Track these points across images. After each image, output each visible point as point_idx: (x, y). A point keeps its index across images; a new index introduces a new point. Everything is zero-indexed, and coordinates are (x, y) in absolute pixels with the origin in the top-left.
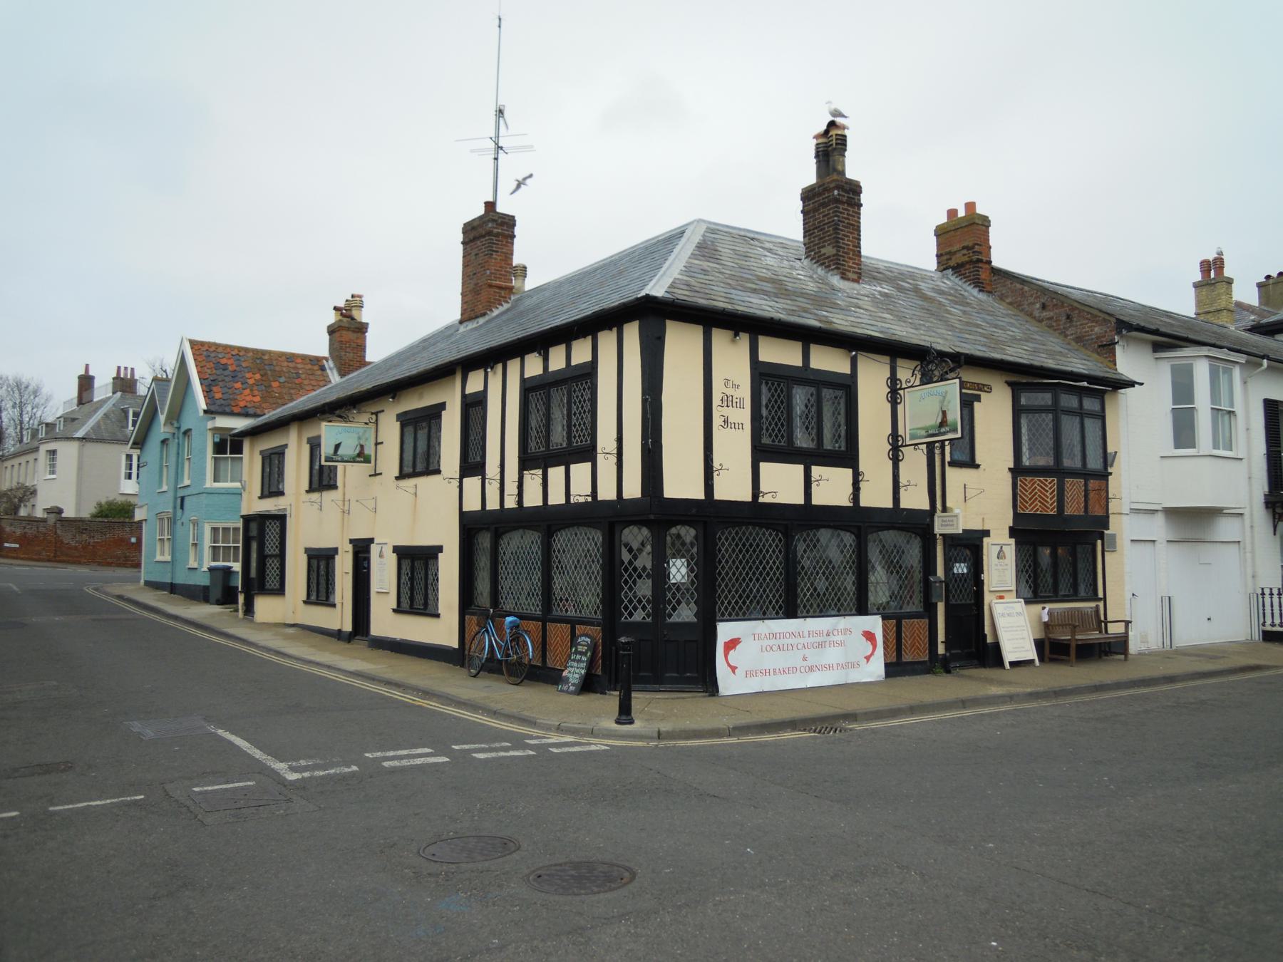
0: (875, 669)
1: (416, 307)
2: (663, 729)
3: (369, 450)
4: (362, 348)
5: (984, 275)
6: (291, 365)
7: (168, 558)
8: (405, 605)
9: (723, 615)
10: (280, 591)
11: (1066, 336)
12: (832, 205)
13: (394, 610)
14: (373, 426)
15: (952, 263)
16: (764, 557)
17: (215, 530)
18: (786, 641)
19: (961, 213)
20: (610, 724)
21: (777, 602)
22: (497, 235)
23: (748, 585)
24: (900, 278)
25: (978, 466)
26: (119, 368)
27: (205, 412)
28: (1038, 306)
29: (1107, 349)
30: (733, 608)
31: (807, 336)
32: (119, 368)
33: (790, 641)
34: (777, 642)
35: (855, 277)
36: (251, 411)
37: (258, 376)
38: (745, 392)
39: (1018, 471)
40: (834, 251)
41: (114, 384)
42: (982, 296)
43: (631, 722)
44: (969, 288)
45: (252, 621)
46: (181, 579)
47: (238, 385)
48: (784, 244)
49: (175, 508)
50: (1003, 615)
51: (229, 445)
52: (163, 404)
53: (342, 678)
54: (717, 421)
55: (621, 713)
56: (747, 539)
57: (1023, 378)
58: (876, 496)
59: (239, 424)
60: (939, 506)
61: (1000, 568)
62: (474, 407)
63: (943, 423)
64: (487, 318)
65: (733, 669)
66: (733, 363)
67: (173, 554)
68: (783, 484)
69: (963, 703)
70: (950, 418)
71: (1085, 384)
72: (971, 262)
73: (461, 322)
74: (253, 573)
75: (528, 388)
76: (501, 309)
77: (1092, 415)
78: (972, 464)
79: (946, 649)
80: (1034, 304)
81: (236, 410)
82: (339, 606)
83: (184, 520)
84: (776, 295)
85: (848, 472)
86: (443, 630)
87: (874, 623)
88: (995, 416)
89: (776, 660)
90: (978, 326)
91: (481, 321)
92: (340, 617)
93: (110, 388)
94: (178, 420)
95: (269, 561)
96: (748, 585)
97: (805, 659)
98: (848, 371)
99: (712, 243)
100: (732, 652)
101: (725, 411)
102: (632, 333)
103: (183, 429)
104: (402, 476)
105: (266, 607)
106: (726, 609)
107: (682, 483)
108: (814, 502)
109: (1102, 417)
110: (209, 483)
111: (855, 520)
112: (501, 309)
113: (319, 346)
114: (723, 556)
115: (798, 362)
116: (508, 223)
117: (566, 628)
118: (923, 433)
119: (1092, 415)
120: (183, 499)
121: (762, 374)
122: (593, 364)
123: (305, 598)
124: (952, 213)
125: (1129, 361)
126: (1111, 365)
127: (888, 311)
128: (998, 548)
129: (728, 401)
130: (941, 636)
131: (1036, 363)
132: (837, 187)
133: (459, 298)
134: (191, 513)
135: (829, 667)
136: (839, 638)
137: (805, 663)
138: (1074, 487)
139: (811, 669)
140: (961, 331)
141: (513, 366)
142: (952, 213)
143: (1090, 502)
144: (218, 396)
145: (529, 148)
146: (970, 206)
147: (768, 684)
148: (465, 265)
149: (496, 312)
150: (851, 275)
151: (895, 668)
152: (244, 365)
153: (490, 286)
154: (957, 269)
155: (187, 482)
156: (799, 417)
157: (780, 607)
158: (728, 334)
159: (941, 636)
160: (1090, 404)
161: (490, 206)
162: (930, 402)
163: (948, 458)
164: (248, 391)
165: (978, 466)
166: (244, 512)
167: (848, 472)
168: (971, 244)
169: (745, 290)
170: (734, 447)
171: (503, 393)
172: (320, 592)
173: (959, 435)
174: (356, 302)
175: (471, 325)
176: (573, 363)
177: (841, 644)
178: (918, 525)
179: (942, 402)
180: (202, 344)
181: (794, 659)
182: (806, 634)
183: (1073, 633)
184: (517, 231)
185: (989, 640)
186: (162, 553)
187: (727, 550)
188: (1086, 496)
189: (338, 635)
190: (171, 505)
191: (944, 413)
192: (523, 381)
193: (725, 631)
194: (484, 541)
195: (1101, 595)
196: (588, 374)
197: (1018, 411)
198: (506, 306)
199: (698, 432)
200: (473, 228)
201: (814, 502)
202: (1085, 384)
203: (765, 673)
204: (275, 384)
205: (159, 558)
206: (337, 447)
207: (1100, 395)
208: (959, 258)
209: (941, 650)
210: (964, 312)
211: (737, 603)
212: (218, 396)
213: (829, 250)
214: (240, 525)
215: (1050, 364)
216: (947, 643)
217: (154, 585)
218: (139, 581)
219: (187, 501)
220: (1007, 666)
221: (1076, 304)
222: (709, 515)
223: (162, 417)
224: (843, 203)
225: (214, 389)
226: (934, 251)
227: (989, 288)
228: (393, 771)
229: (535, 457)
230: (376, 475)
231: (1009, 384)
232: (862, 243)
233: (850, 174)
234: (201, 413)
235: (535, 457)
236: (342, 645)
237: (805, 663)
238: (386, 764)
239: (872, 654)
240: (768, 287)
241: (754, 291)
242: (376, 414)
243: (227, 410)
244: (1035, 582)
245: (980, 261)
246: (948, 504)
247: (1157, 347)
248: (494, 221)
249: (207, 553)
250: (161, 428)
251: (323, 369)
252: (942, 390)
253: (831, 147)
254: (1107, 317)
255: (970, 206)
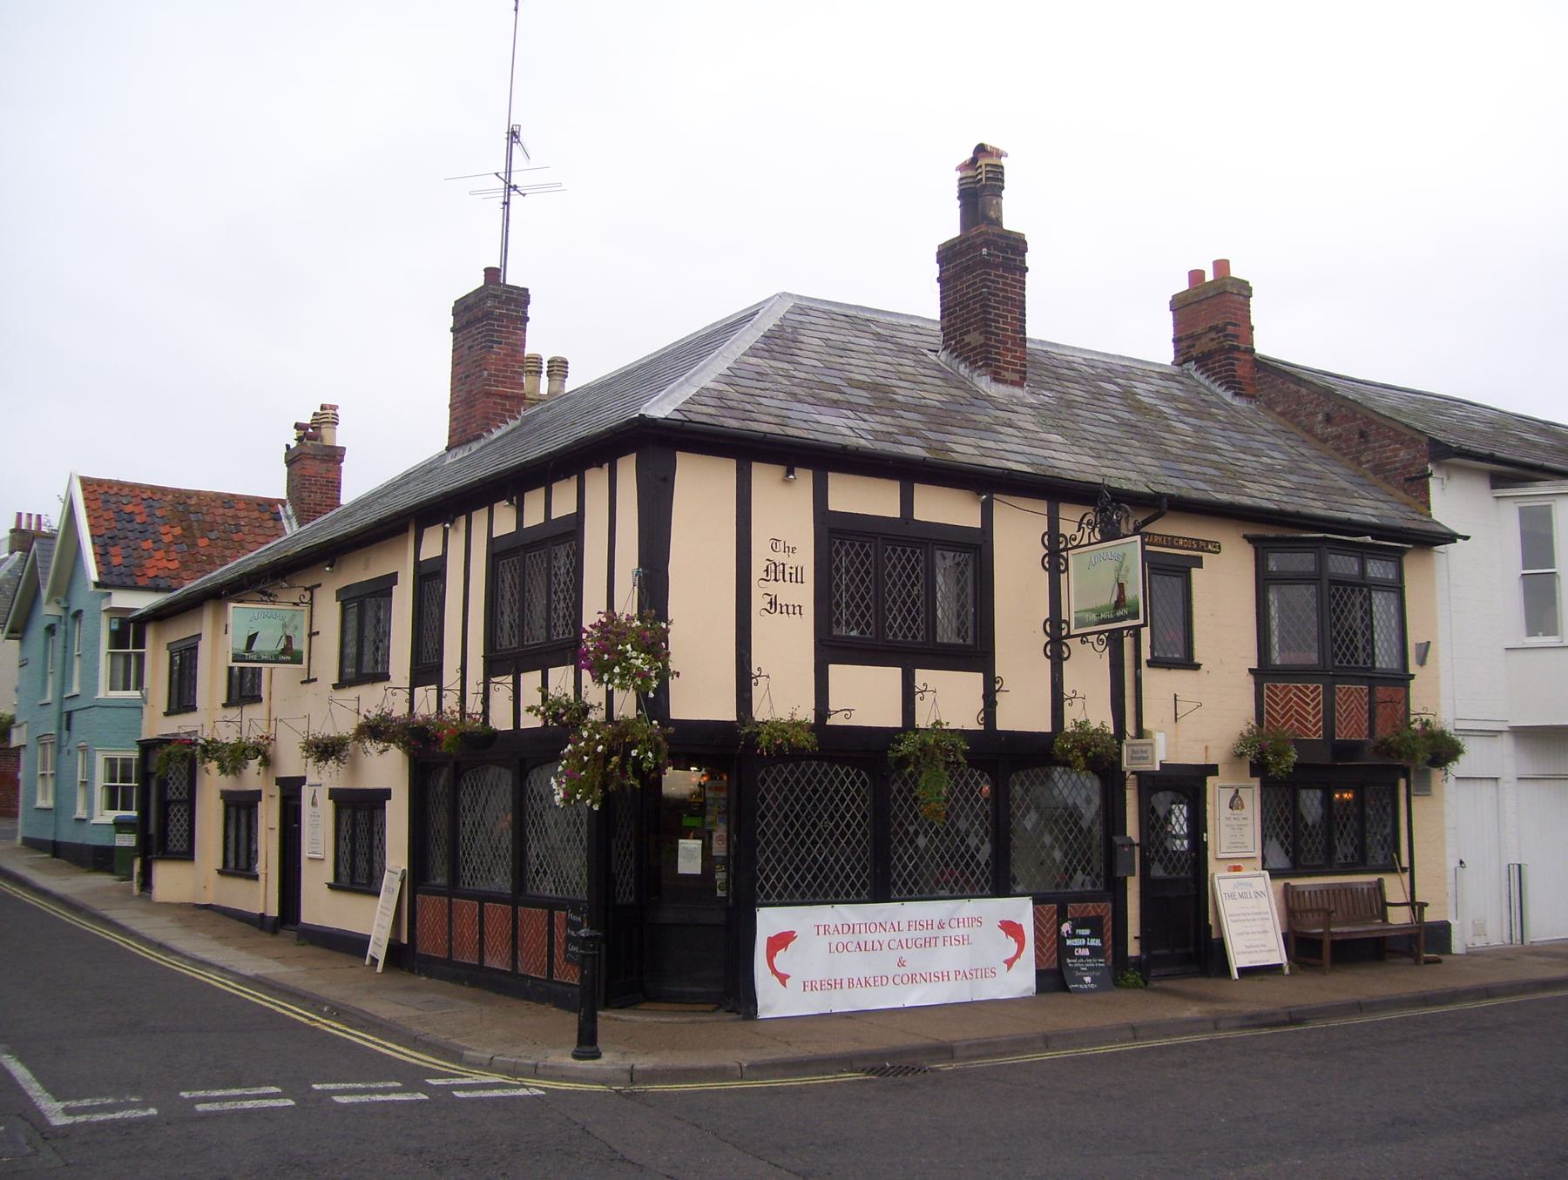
0: (1021, 980)
1: (399, 431)
2: (638, 1067)
3: (300, 644)
4: (335, 485)
5: (1242, 370)
6: (230, 512)
7: (50, 803)
8: (345, 879)
9: (768, 896)
10: (188, 855)
11: (1360, 464)
12: (983, 267)
13: (330, 886)
14: (306, 608)
15: (1194, 353)
16: (837, 808)
17: (111, 762)
18: (870, 937)
19: (1209, 277)
20: (564, 1058)
21: (858, 877)
22: (501, 317)
23: (809, 852)
24: (1099, 383)
25: (1197, 667)
26: (20, 515)
27: (97, 585)
28: (1320, 417)
29: (1417, 486)
30: (785, 887)
31: (908, 473)
32: (20, 515)
33: (876, 936)
34: (854, 938)
35: (1016, 377)
36: (163, 583)
37: (177, 531)
38: (805, 558)
39: (1263, 673)
40: (981, 339)
41: (12, 539)
42: (1238, 403)
43: (596, 1055)
44: (1220, 391)
45: (149, 899)
46: (67, 835)
47: (148, 544)
48: (915, 326)
49: (60, 728)
50: (1232, 896)
51: (129, 631)
52: (46, 573)
53: (230, 986)
54: (758, 602)
55: (580, 1043)
56: (809, 782)
57: (1272, 531)
58: (1023, 711)
59: (142, 602)
60: (1130, 728)
61: (1234, 827)
62: (430, 577)
63: (1120, 602)
64: (482, 442)
65: (783, 978)
66: (786, 512)
67: (57, 797)
68: (867, 696)
69: (1135, 1032)
70: (1129, 595)
71: (1369, 539)
72: (1221, 350)
73: (448, 449)
74: (153, 829)
75: (499, 552)
76: (505, 429)
77: (1382, 586)
78: (1188, 663)
79: (1142, 948)
80: (1314, 414)
81: (142, 582)
82: (262, 878)
83: (71, 746)
84: (870, 410)
85: (977, 678)
86: (375, 918)
87: (1021, 910)
88: (1225, 590)
89: (854, 965)
90: (1214, 450)
91: (475, 446)
92: (262, 897)
93: (6, 546)
94: (67, 599)
95: (173, 810)
96: (809, 852)
97: (901, 964)
98: (976, 522)
99: (790, 331)
100: (781, 953)
101: (773, 587)
102: (627, 469)
103: (72, 611)
104: (343, 683)
105: (170, 880)
106: (774, 887)
107: (700, 695)
108: (1000, 726)
109: (1397, 588)
110: (104, 692)
111: (999, 755)
112: (505, 429)
113: (272, 483)
114: (769, 808)
115: (892, 510)
116: (520, 298)
117: (541, 913)
118: (1094, 617)
119: (1382, 586)
120: (69, 714)
121: (833, 532)
122: (579, 517)
123: (220, 867)
124: (1196, 276)
125: (1452, 501)
126: (1422, 508)
127: (1059, 428)
128: (1231, 793)
129: (776, 571)
130: (1133, 928)
131: (1289, 508)
132: (987, 244)
133: (1254, 321)
134: (78, 737)
135: (943, 976)
136: (959, 932)
137: (902, 971)
138: (1351, 696)
139: (912, 978)
140: (1178, 459)
141: (480, 518)
142: (1196, 276)
143: (1379, 720)
144: (115, 561)
145: (556, 187)
146: (1221, 266)
147: (841, 1002)
148: (455, 364)
149: (497, 433)
150: (1008, 375)
151: (1053, 978)
152: (158, 513)
153: (489, 394)
154: (1203, 361)
155: (76, 690)
156: (889, 593)
157: (864, 885)
158: (777, 471)
159: (1133, 928)
160: (1377, 569)
161: (492, 274)
162: (1108, 568)
163: (1146, 655)
164: (158, 555)
165: (1197, 667)
166: (145, 736)
167: (977, 678)
168: (1220, 323)
169: (819, 402)
170: (786, 644)
171: (463, 556)
172: (239, 863)
173: (1141, 621)
174: (327, 416)
175: (461, 453)
176: (554, 517)
177: (963, 940)
178: (1101, 759)
179: (1118, 570)
180: (100, 483)
181: (885, 963)
182: (904, 926)
183: (1327, 925)
184: (532, 311)
185: (1214, 936)
186: (45, 798)
187: (775, 799)
188: (1372, 712)
189: (259, 922)
190: (55, 724)
191: (1121, 586)
192: (492, 541)
193: (769, 920)
194: (442, 781)
195: (1405, 863)
196: (570, 532)
197: (1264, 581)
198: (512, 424)
199: (734, 620)
200: (468, 308)
201: (1000, 726)
202: (1369, 539)
203: (835, 984)
204: (203, 542)
205: (40, 803)
206: (252, 639)
207: (1397, 557)
208: (1205, 344)
209: (1133, 949)
210: (1198, 429)
211: (791, 878)
212: (115, 561)
213: (975, 338)
214: (134, 754)
215: (1318, 508)
216: (1143, 938)
217: (32, 844)
218: (14, 838)
219: (76, 716)
220: (1235, 975)
221: (1372, 416)
222: (727, 748)
223: (45, 593)
224: (997, 266)
225: (112, 550)
226: (1169, 333)
227: (1250, 390)
228: (207, 1116)
229: (503, 660)
230: (309, 681)
231: (1250, 539)
232: (1027, 326)
233: (1010, 223)
234: (92, 588)
235: (503, 660)
236: (267, 937)
237: (902, 971)
238: (200, 1107)
239: (1018, 955)
240: (860, 397)
241: (835, 404)
242: (311, 589)
243: (128, 581)
244: (1295, 844)
245: (1237, 349)
246: (1145, 726)
247: (1499, 481)
248: (495, 296)
249: (100, 797)
250: (48, 610)
251: (276, 518)
252: (1120, 550)
253: (981, 183)
254: (1417, 436)
255: (1221, 266)
